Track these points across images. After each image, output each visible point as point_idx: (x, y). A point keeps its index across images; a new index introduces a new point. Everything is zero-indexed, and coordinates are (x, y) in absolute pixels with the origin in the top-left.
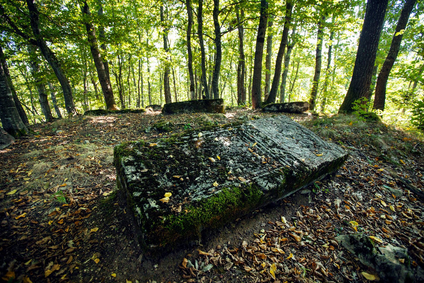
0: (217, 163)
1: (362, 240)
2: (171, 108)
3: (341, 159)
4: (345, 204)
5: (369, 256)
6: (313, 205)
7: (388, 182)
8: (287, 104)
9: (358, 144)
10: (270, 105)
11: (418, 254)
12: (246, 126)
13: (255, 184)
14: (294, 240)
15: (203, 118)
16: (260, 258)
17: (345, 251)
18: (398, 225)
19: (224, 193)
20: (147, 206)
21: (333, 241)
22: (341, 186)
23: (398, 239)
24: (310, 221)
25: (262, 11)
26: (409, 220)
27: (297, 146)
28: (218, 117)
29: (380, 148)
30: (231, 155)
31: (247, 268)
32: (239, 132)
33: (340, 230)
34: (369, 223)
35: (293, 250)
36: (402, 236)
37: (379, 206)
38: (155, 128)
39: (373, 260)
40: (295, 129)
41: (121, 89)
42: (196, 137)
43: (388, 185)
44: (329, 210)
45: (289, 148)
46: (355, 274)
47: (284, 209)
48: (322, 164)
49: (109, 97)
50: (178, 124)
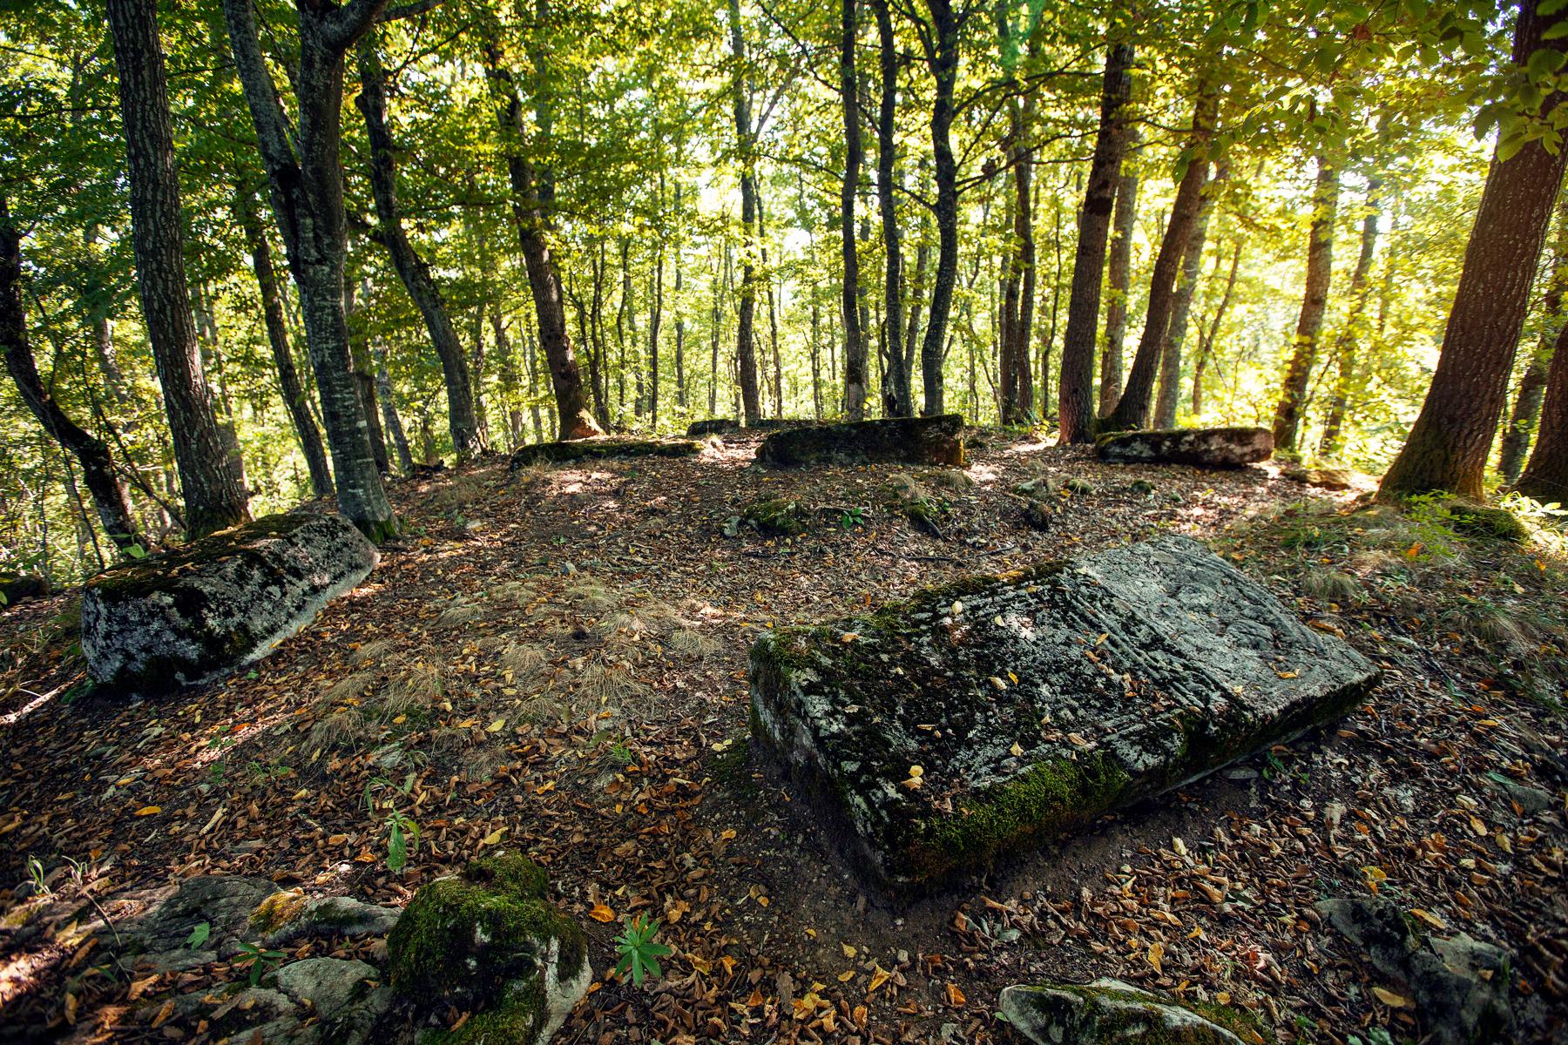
0: (1012, 692)
1: (1381, 914)
2: (790, 446)
3: (1355, 687)
4: (1358, 817)
5: (1396, 952)
6: (1263, 814)
7: (1506, 763)
8: (1192, 437)
9: (1426, 629)
10: (1129, 436)
11: (1545, 969)
12: (1074, 576)
13: (1112, 756)
14: (1206, 899)
15: (900, 488)
16: (1125, 928)
17: (1338, 936)
18: (1510, 890)
19: (1040, 774)
20: (880, 794)
21: (1306, 911)
22: (1351, 766)
23: (1496, 926)
24: (1251, 858)
25: (1108, 107)
26: (1549, 881)
27: (1222, 645)
28: (946, 482)
29: (1503, 646)
30: (1042, 671)
31: (1097, 946)
32: (1057, 597)
33: (1330, 885)
34: (1421, 876)
35: (1203, 920)
36: (1514, 919)
37: (1464, 832)
38: (752, 522)
39: (1405, 963)
40: (1219, 584)
41: (597, 354)
42: (947, 615)
43: (1504, 772)
44: (1306, 831)
45: (1199, 650)
46: (1354, 990)
47: (1180, 817)
48: (1294, 704)
49: (570, 388)
50: (823, 510)
